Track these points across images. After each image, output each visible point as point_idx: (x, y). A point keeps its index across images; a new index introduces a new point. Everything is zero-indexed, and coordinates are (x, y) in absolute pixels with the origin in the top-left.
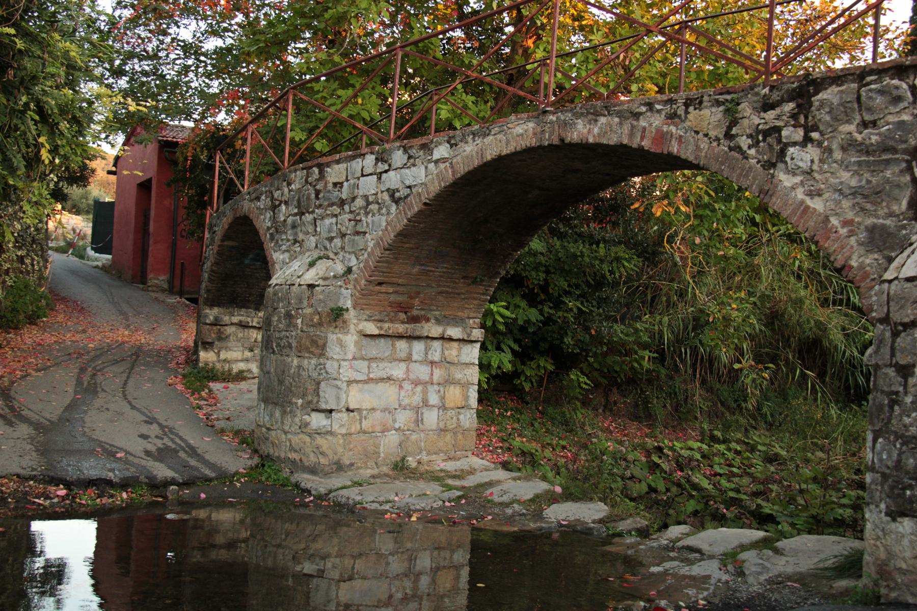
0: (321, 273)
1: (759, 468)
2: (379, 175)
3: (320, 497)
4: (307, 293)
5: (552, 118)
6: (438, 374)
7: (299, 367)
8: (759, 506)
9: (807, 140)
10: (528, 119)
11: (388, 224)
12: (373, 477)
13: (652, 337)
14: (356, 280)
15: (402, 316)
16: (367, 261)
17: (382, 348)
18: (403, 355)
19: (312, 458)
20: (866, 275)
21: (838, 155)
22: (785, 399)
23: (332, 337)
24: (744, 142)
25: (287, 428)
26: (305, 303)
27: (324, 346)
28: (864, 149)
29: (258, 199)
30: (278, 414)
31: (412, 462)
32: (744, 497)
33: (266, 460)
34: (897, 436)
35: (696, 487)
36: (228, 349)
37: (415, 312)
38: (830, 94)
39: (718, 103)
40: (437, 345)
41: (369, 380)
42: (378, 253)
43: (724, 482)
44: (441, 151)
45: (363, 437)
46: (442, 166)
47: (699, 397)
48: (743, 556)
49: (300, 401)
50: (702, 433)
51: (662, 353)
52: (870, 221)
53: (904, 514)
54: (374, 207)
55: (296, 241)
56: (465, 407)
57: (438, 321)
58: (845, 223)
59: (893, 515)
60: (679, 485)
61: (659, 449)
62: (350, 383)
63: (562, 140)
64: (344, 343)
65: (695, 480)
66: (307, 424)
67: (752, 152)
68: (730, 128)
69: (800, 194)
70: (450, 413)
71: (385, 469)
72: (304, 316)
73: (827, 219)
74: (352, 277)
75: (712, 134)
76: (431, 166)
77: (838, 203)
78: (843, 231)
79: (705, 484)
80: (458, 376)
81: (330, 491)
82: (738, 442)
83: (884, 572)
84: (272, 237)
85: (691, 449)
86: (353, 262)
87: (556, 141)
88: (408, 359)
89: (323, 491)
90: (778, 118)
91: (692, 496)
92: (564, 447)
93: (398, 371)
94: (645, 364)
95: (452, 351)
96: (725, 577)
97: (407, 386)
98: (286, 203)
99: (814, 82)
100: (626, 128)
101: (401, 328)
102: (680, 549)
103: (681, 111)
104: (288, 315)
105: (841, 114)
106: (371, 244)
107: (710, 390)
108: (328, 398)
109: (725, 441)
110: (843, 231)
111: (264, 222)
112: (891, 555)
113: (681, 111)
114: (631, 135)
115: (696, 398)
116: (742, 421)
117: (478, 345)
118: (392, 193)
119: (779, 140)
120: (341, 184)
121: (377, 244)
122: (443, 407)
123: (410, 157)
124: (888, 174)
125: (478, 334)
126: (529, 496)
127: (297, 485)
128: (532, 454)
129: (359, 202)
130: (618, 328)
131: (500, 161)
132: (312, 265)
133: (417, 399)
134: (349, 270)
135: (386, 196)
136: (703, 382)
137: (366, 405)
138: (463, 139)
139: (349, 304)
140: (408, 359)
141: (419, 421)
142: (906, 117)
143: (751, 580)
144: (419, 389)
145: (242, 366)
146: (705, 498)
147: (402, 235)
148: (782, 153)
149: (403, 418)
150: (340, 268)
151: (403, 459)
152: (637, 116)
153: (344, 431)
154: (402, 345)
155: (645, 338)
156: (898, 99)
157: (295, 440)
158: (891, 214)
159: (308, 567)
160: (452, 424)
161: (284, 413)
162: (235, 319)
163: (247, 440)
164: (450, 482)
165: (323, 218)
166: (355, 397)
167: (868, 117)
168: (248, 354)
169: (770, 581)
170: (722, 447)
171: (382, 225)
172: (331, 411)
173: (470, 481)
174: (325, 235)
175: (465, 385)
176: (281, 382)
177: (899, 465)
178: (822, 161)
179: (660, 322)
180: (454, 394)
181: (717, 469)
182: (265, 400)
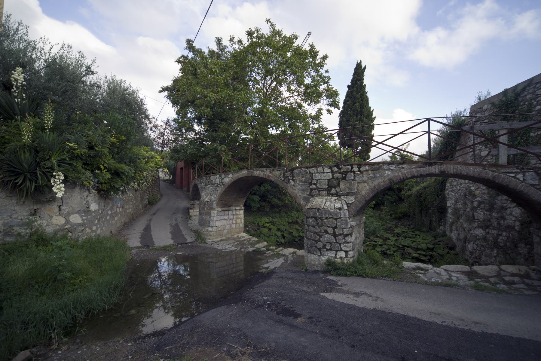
17: (223, 213)
40: (234, 211)
44: (231, 176)
64: (214, 213)
93: (226, 217)
95: (238, 212)
105: (298, 175)
108: (212, 224)
111: (199, 186)
125: (243, 208)
131: (241, 179)
133: (231, 222)
140: (228, 215)
147: (224, 191)
148: (289, 181)
154: (227, 212)
166: (217, 224)
171: (220, 190)
175: (241, 219)
180: (239, 221)
182: (200, 225)
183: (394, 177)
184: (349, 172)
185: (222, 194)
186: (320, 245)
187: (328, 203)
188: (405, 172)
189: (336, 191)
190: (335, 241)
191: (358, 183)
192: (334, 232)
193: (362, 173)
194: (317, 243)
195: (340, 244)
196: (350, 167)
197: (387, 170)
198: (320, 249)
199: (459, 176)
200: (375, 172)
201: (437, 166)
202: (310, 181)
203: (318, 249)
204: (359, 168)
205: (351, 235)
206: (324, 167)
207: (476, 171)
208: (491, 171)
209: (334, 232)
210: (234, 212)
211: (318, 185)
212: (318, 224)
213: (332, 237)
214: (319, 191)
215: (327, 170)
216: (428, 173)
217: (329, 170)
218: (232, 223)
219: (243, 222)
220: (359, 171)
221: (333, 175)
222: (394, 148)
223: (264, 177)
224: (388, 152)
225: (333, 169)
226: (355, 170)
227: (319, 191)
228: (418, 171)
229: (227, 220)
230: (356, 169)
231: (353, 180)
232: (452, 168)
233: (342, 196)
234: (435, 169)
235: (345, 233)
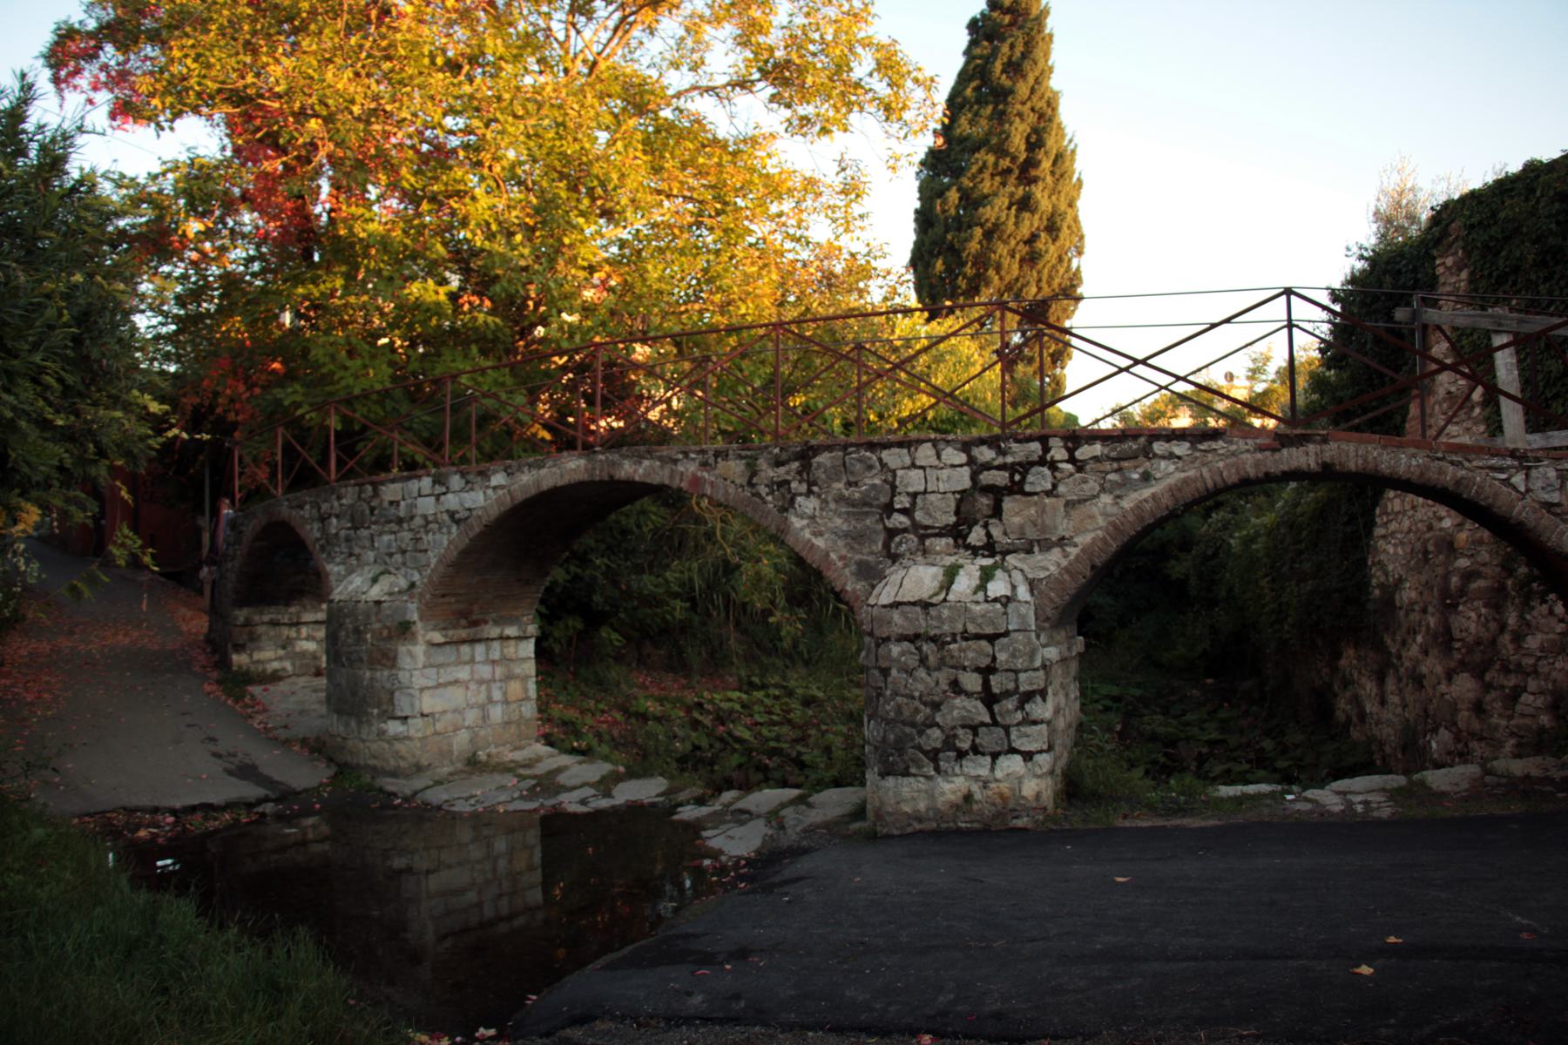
0: (386, 589)
1: (797, 714)
2: (438, 497)
3: (406, 799)
4: (375, 609)
5: (601, 457)
6: (499, 671)
7: (372, 679)
8: (799, 753)
9: (809, 493)
10: (580, 456)
11: (450, 542)
12: (451, 774)
13: (682, 585)
14: (421, 595)
15: (464, 622)
16: (430, 577)
17: (449, 654)
18: (467, 658)
19: (392, 762)
20: (857, 598)
21: (832, 506)
22: (821, 633)
23: (402, 649)
24: (763, 490)
25: (364, 736)
26: (373, 619)
27: (395, 659)
28: (850, 502)
29: (301, 507)
30: (353, 724)
31: (482, 755)
32: (785, 746)
33: (343, 770)
34: (883, 719)
35: (739, 740)
36: (260, 649)
37: (474, 617)
38: (823, 458)
39: (741, 457)
40: (496, 645)
41: (439, 685)
42: (441, 569)
43: (765, 731)
44: (498, 479)
45: (437, 738)
46: (500, 492)
47: (734, 643)
48: (783, 813)
49: (375, 711)
50: (740, 680)
51: (692, 600)
52: (858, 557)
53: (889, 774)
54: (434, 526)
55: (351, 555)
56: (527, 699)
57: (496, 623)
58: (842, 558)
59: (883, 775)
60: (721, 739)
61: (700, 705)
62: (422, 690)
63: (612, 477)
64: (415, 657)
65: (737, 733)
66: (384, 732)
67: (769, 498)
68: (751, 478)
69: (807, 534)
70: (514, 706)
71: (459, 766)
72: (373, 632)
73: (827, 555)
74: (415, 591)
75: (738, 481)
76: (490, 492)
77: (835, 542)
78: (840, 564)
79: (747, 735)
80: (518, 671)
81: (416, 793)
82: (776, 686)
83: (879, 815)
84: (323, 549)
85: (730, 700)
86: (416, 577)
87: (606, 478)
88: (472, 661)
89: (408, 792)
90: (788, 473)
91: (735, 750)
92: (603, 712)
93: (463, 673)
94: (677, 614)
95: (511, 649)
96: (770, 832)
97: (473, 686)
98: (337, 516)
99: (812, 448)
100: (667, 471)
101: (463, 633)
102: (733, 812)
103: (711, 461)
104: (357, 631)
105: (834, 475)
106: (434, 561)
107: (745, 632)
108: (403, 705)
109: (763, 687)
110: (840, 564)
111: (312, 532)
112: (882, 803)
113: (711, 461)
114: (672, 477)
115: (732, 641)
116: (779, 663)
117: (533, 641)
118: (452, 514)
119: (789, 490)
120: (398, 503)
121: (440, 561)
122: (506, 702)
123: (467, 482)
124: (868, 522)
126: (597, 778)
127: (381, 790)
128: (573, 723)
129: (418, 521)
130: (647, 579)
131: (555, 492)
132: (375, 580)
133: (482, 697)
134: (413, 585)
135: (446, 517)
136: (737, 624)
137: (439, 708)
138: (520, 469)
139: (415, 617)
140: (472, 661)
141: (485, 717)
142: (877, 481)
143: (790, 831)
144: (483, 687)
145: (276, 665)
146: (748, 751)
147: (464, 553)
148: (792, 501)
149: (472, 716)
150: (403, 583)
151: (475, 754)
152: (675, 461)
153: (420, 735)
154: (465, 649)
155: (676, 589)
156: (870, 467)
157: (374, 747)
158: (872, 553)
159: (398, 863)
160: (515, 717)
161: (360, 723)
162: (266, 618)
163: (318, 747)
164: (522, 771)
165: (380, 534)
166: (428, 703)
167: (852, 479)
168: (281, 652)
169: (805, 831)
170: (759, 694)
171: (442, 544)
172: (406, 718)
173: (541, 769)
174: (383, 550)
175: (525, 679)
176: (354, 694)
177: (884, 739)
178: (822, 509)
179: (690, 570)
180: (515, 688)
181: (758, 718)
183: (1186, 481)
184: (1032, 464)
185: (452, 565)
186: (935, 737)
187: (964, 583)
188: (1221, 464)
189: (989, 535)
190: (987, 719)
191: (1068, 504)
192: (986, 684)
193: (1080, 469)
194: (921, 733)
195: (1007, 729)
196: (1035, 446)
197: (1163, 457)
198: (934, 755)
199: (1405, 485)
200: (1125, 464)
201: (1311, 447)
202: (884, 499)
203: (926, 753)
204: (1071, 451)
205: (1043, 693)
206: (941, 445)
207: (1414, 462)
208: (1452, 463)
209: (986, 684)
210: (496, 650)
211: (918, 515)
212: (923, 661)
213: (980, 705)
214: (922, 538)
215: (953, 456)
216: (1285, 468)
217: (962, 458)
218: (490, 700)
219: (533, 693)
220: (1072, 460)
221: (974, 477)
222: (1178, 378)
223: (676, 483)
224: (1161, 388)
225: (976, 451)
226: (1058, 457)
227: (922, 538)
228: (1257, 464)
229: (465, 685)
230: (1058, 452)
231: (1049, 493)
232: (1352, 454)
233: (1009, 552)
234: (1303, 457)
235: (1024, 688)
